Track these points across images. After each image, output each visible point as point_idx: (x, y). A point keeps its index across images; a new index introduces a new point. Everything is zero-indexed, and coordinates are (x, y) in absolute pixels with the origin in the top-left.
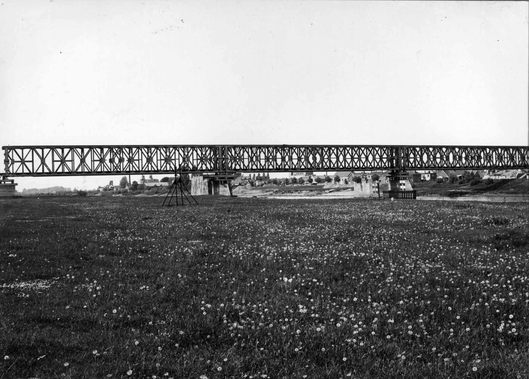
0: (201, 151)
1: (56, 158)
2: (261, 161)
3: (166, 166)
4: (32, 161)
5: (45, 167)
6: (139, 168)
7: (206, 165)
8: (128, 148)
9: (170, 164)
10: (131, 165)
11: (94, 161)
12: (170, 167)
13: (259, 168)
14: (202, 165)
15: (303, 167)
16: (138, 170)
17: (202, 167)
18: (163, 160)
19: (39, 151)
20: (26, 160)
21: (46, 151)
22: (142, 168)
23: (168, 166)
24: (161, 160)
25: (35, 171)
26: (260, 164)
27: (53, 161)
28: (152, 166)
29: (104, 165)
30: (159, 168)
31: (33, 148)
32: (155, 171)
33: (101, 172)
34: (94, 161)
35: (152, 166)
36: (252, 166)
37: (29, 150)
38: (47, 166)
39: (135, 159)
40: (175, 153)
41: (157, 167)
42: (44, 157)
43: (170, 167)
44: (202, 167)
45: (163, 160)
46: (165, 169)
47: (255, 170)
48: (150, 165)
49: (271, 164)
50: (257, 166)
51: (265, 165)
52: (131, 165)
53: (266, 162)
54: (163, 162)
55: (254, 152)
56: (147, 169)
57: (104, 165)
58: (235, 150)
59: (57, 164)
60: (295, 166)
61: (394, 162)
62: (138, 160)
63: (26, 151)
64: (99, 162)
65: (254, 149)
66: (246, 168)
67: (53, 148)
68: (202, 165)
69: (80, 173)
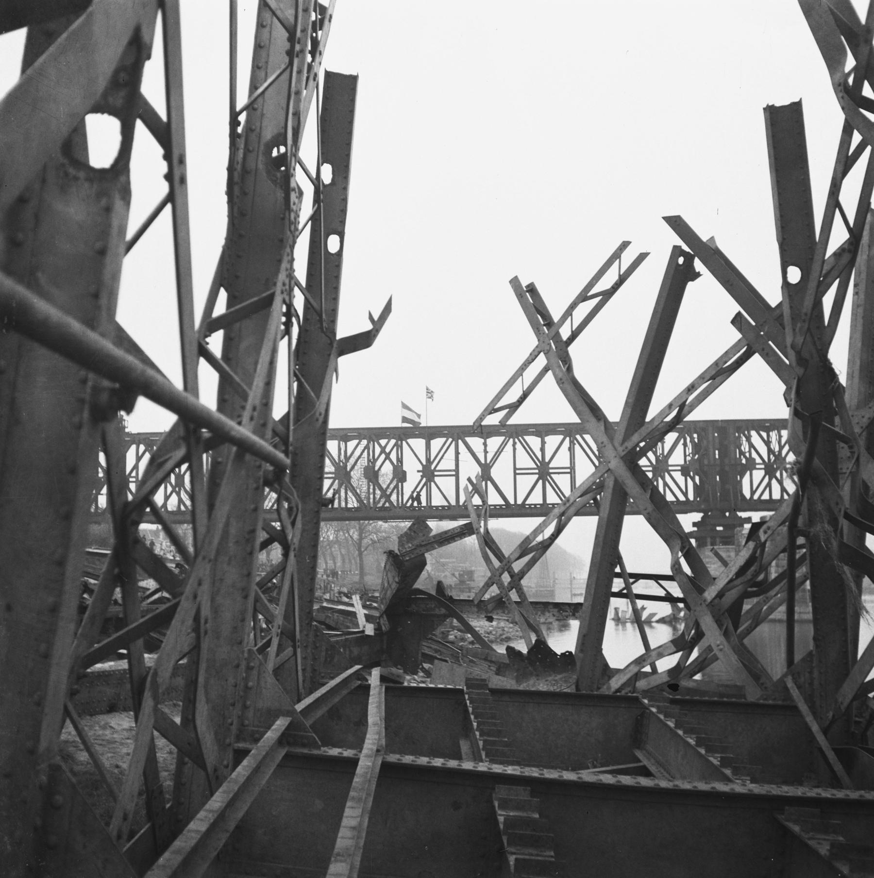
5: (548, 488)
14: (770, 480)
56: (766, 496)
63: (553, 441)
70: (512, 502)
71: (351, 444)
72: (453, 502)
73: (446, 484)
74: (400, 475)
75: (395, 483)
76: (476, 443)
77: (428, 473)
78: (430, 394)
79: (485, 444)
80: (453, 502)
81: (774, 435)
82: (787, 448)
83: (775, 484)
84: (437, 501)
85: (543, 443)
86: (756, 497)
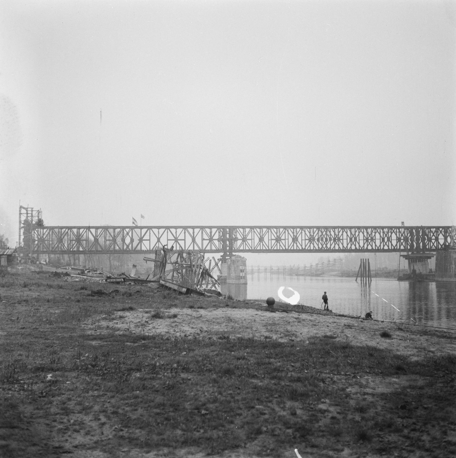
0: (334, 232)
1: (205, 237)
2: (393, 241)
3: (310, 246)
4: (185, 240)
5: (195, 244)
6: (268, 247)
7: (338, 245)
8: (259, 228)
9: (296, 244)
10: (261, 243)
11: (251, 240)
12: (314, 246)
13: (390, 248)
14: (310, 244)
15: (433, 248)
16: (267, 249)
17: (334, 247)
18: (307, 240)
19: (191, 230)
20: (179, 238)
21: (196, 230)
22: (272, 248)
23: (312, 245)
24: (305, 240)
25: (186, 249)
26: (392, 245)
27: (203, 239)
28: (297, 246)
29: (246, 244)
30: (287, 248)
31: (185, 228)
32: (266, 250)
33: (260, 250)
34: (251, 240)
35: (297, 246)
36: (384, 246)
37: (182, 229)
38: (197, 245)
39: (282, 238)
40: (301, 233)
41: (285, 246)
42: (195, 236)
43: (314, 246)
44: (334, 247)
45: (307, 240)
46: (309, 248)
47: (386, 250)
48: (295, 244)
49: (369, 244)
50: (388, 246)
51: (396, 245)
52: (261, 243)
53: (397, 243)
54: (307, 241)
55: (370, 233)
56: (292, 248)
57: (246, 244)
58: (367, 230)
59: (205, 243)
60: (394, 247)
61: (421, 244)
62: (285, 240)
63: (179, 230)
64: (241, 241)
65: (369, 230)
66: (378, 248)
67: (202, 228)
68: (335, 244)
69: (242, 250)
70: (184, 249)
71: (45, 230)
72: (149, 249)
73: (146, 243)
74: (132, 240)
75: (292, 244)
76: (156, 231)
77: (141, 240)
78: (142, 217)
79: (194, 231)
80: (149, 249)
81: (312, 230)
82: (409, 235)
83: (295, 244)
84: (144, 248)
85: (194, 231)
86: (289, 248)
